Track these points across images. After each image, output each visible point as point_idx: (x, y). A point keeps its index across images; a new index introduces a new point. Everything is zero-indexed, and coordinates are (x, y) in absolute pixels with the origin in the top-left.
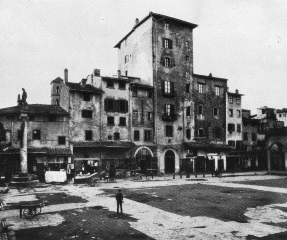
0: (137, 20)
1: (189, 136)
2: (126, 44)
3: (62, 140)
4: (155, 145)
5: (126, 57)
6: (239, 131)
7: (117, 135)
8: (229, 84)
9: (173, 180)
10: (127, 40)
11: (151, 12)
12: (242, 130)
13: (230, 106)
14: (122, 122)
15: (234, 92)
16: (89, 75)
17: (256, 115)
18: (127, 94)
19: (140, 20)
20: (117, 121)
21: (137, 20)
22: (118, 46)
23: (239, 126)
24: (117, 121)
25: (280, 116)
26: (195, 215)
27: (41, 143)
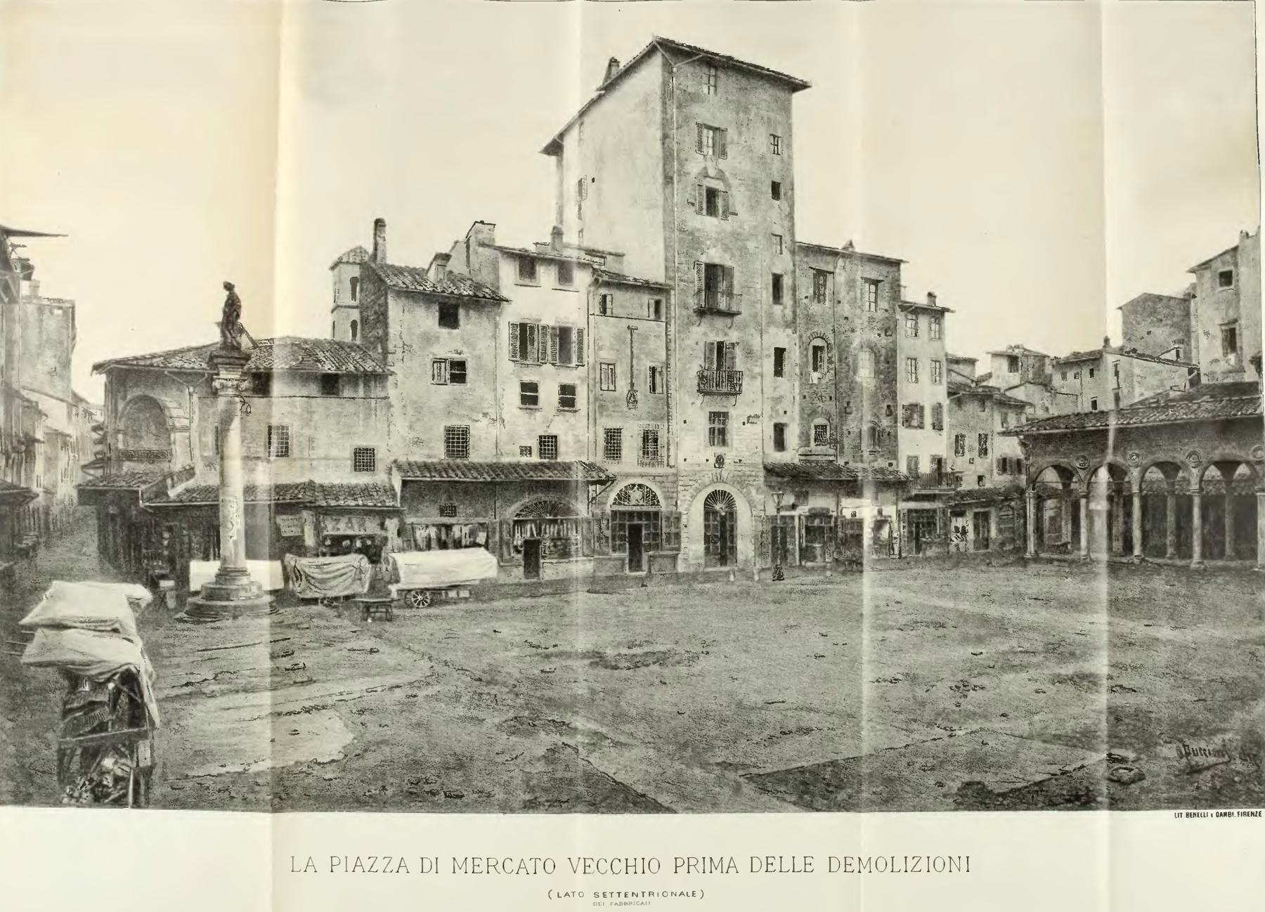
0: (613, 62)
1: (780, 444)
2: (580, 140)
3: (364, 459)
4: (673, 470)
5: (580, 182)
6: (938, 426)
7: (548, 444)
8: (905, 273)
9: (708, 578)
10: (586, 127)
11: (440, 324)
12: (946, 420)
13: (262, 488)
14: (567, 397)
15: (923, 301)
16: (456, 242)
17: (990, 375)
18: (349, 462)
19: (623, 64)
20: (549, 395)
21: (613, 62)
22: (555, 148)
23: (938, 409)
24: (549, 395)
25: (1064, 377)
26: (1040, 805)
27: (870, 545)
